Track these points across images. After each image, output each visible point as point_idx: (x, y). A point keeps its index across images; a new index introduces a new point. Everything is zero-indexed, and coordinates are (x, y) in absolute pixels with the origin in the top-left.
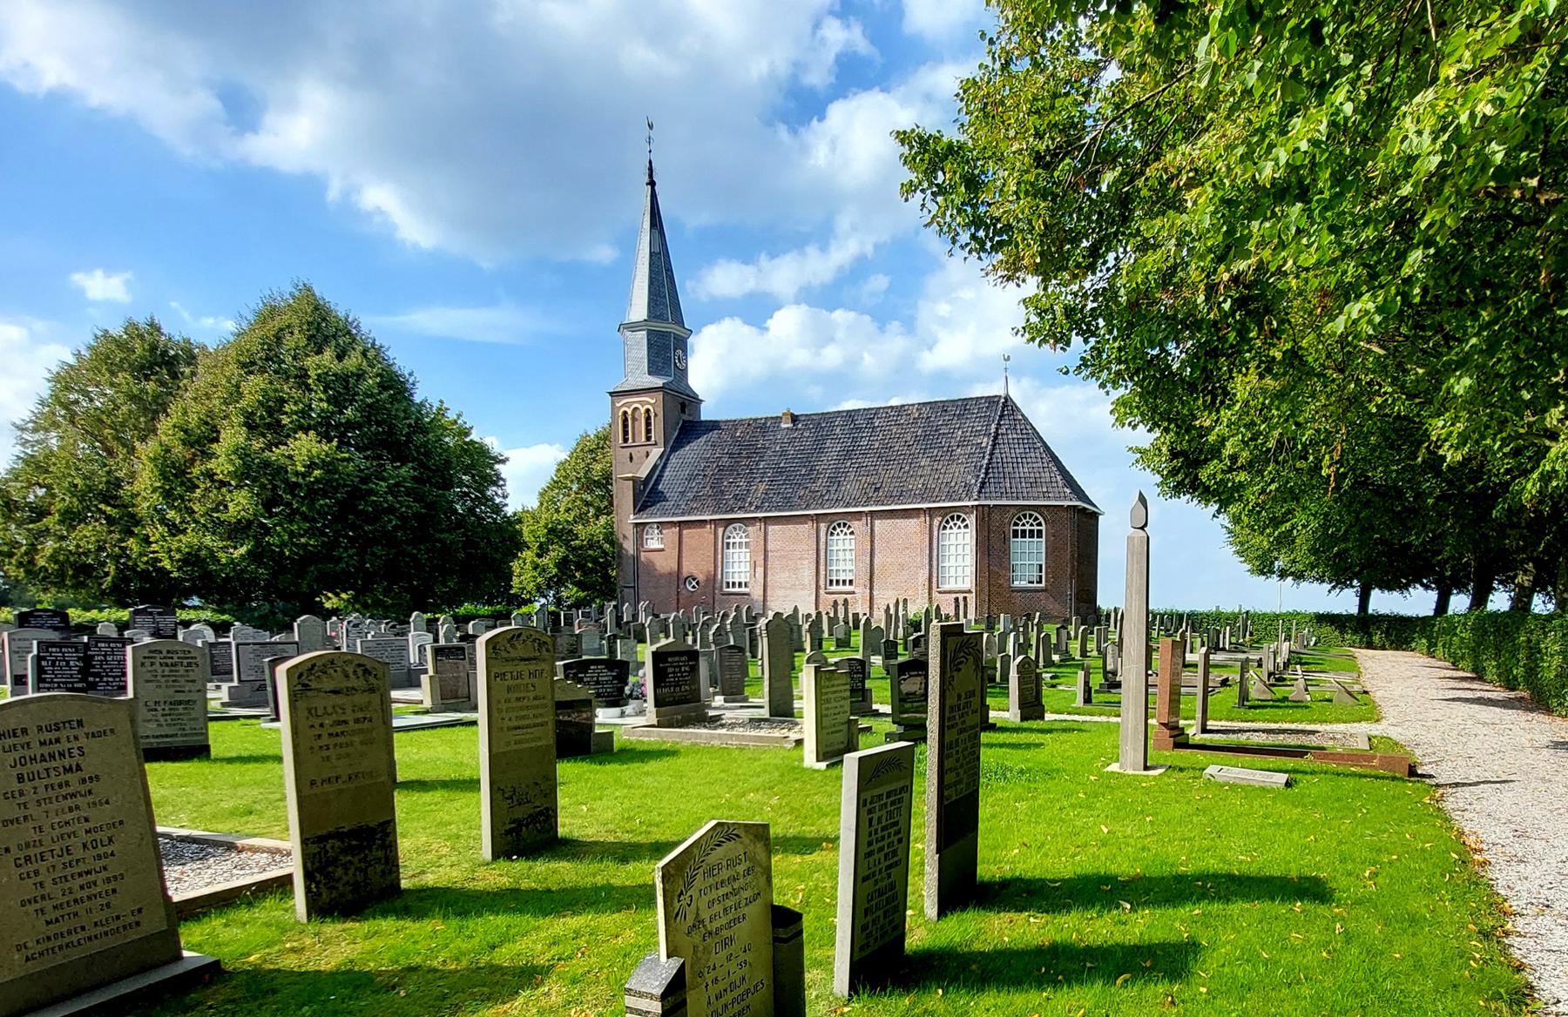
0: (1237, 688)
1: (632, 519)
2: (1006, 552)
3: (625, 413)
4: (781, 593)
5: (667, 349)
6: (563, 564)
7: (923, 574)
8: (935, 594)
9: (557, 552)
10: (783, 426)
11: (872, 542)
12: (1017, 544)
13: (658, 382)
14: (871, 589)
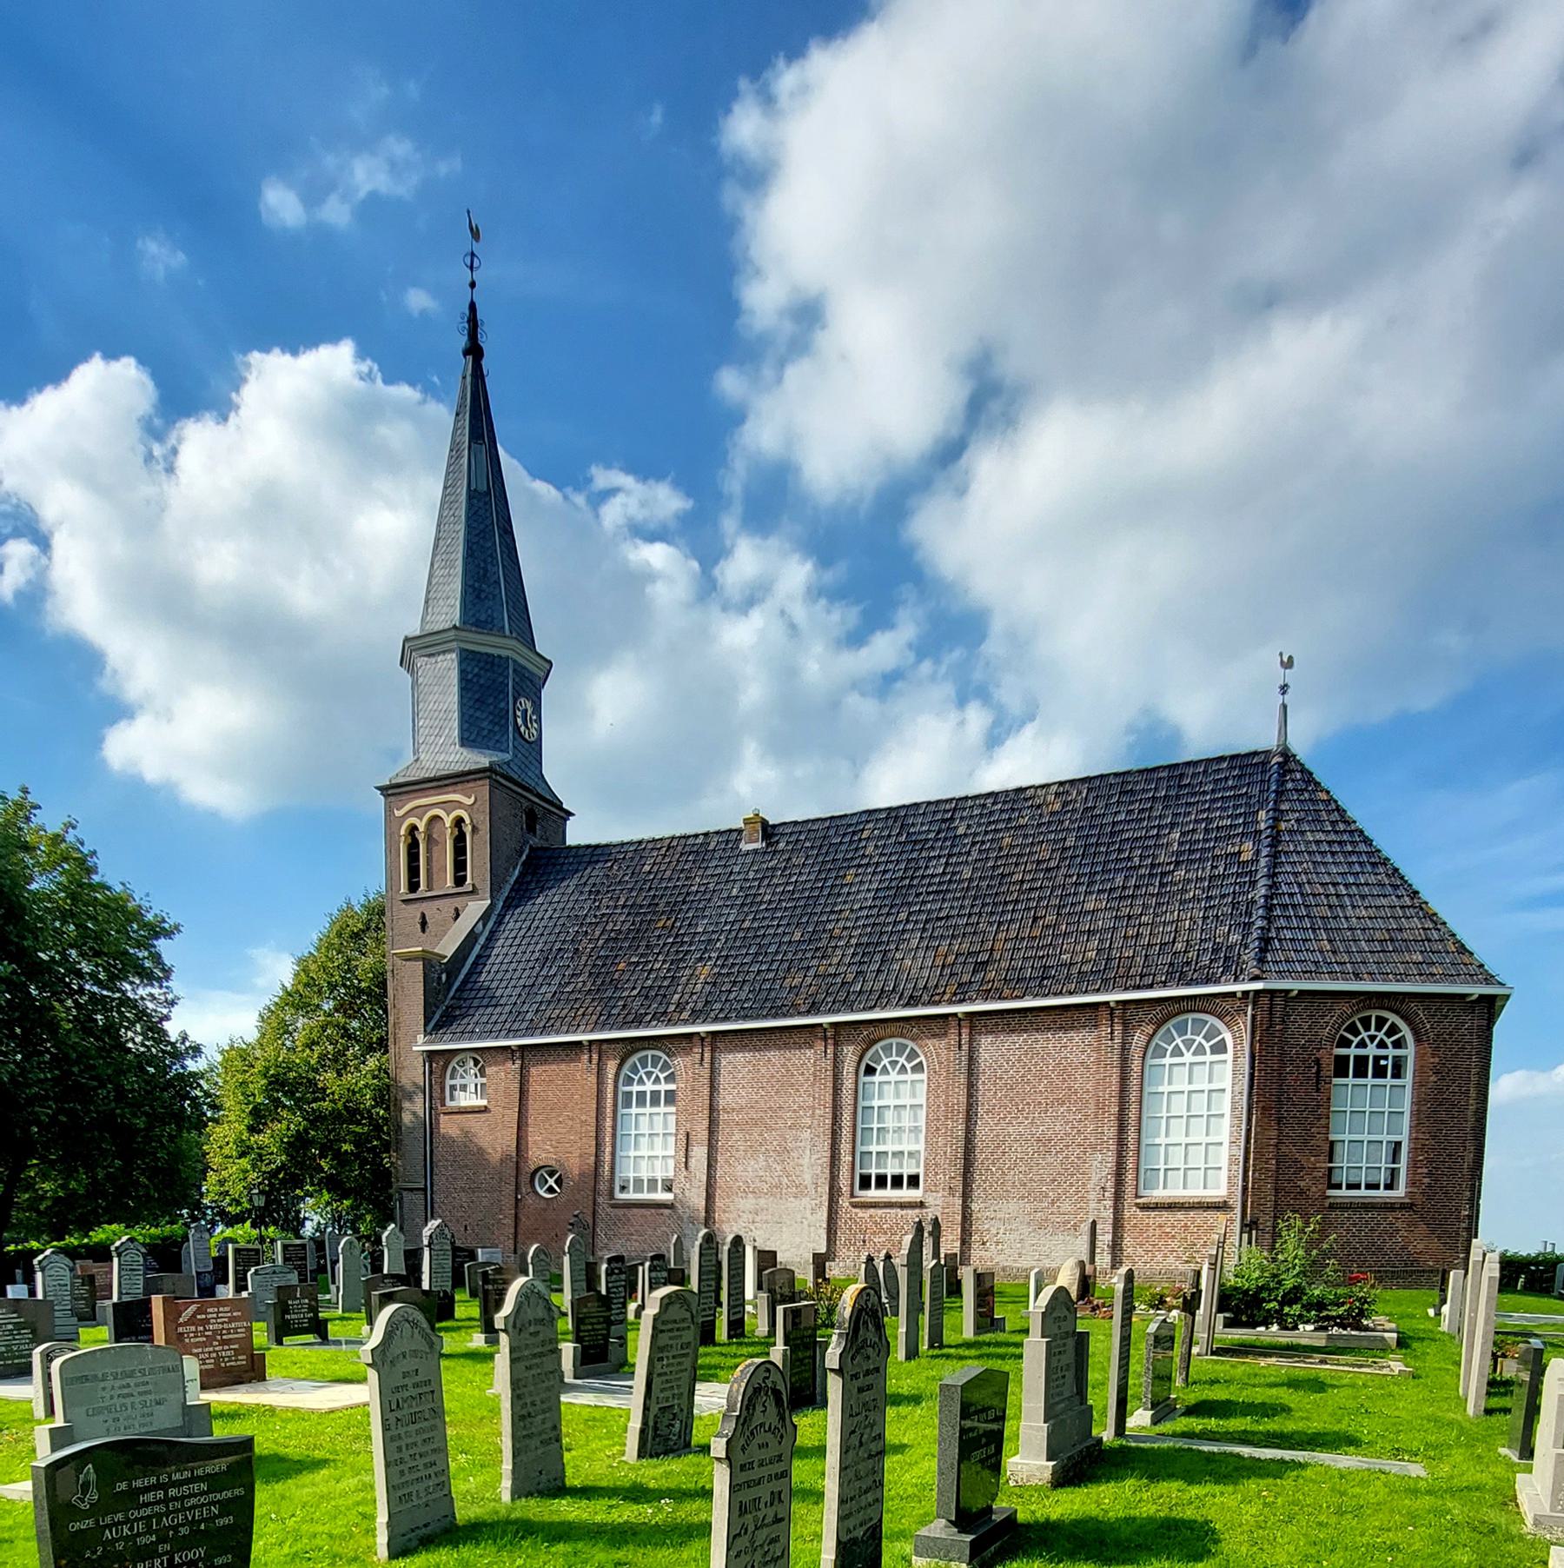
0: (1525, 1390)
1: (421, 1044)
2: (1320, 1112)
3: (414, 828)
4: (748, 1203)
5: (498, 682)
6: (297, 1145)
7: (1101, 1167)
8: (1130, 1212)
9: (289, 1123)
10: (745, 847)
11: (971, 1087)
12: (1351, 1094)
13: (480, 759)
14: (966, 1196)
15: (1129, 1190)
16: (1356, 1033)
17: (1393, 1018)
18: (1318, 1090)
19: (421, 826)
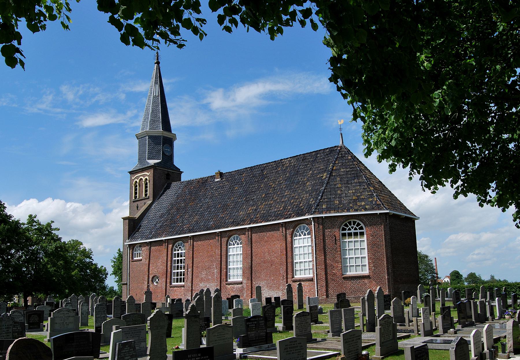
15: (290, 276)
16: (347, 226)
17: (358, 221)
18: (336, 244)
19: (138, 181)
